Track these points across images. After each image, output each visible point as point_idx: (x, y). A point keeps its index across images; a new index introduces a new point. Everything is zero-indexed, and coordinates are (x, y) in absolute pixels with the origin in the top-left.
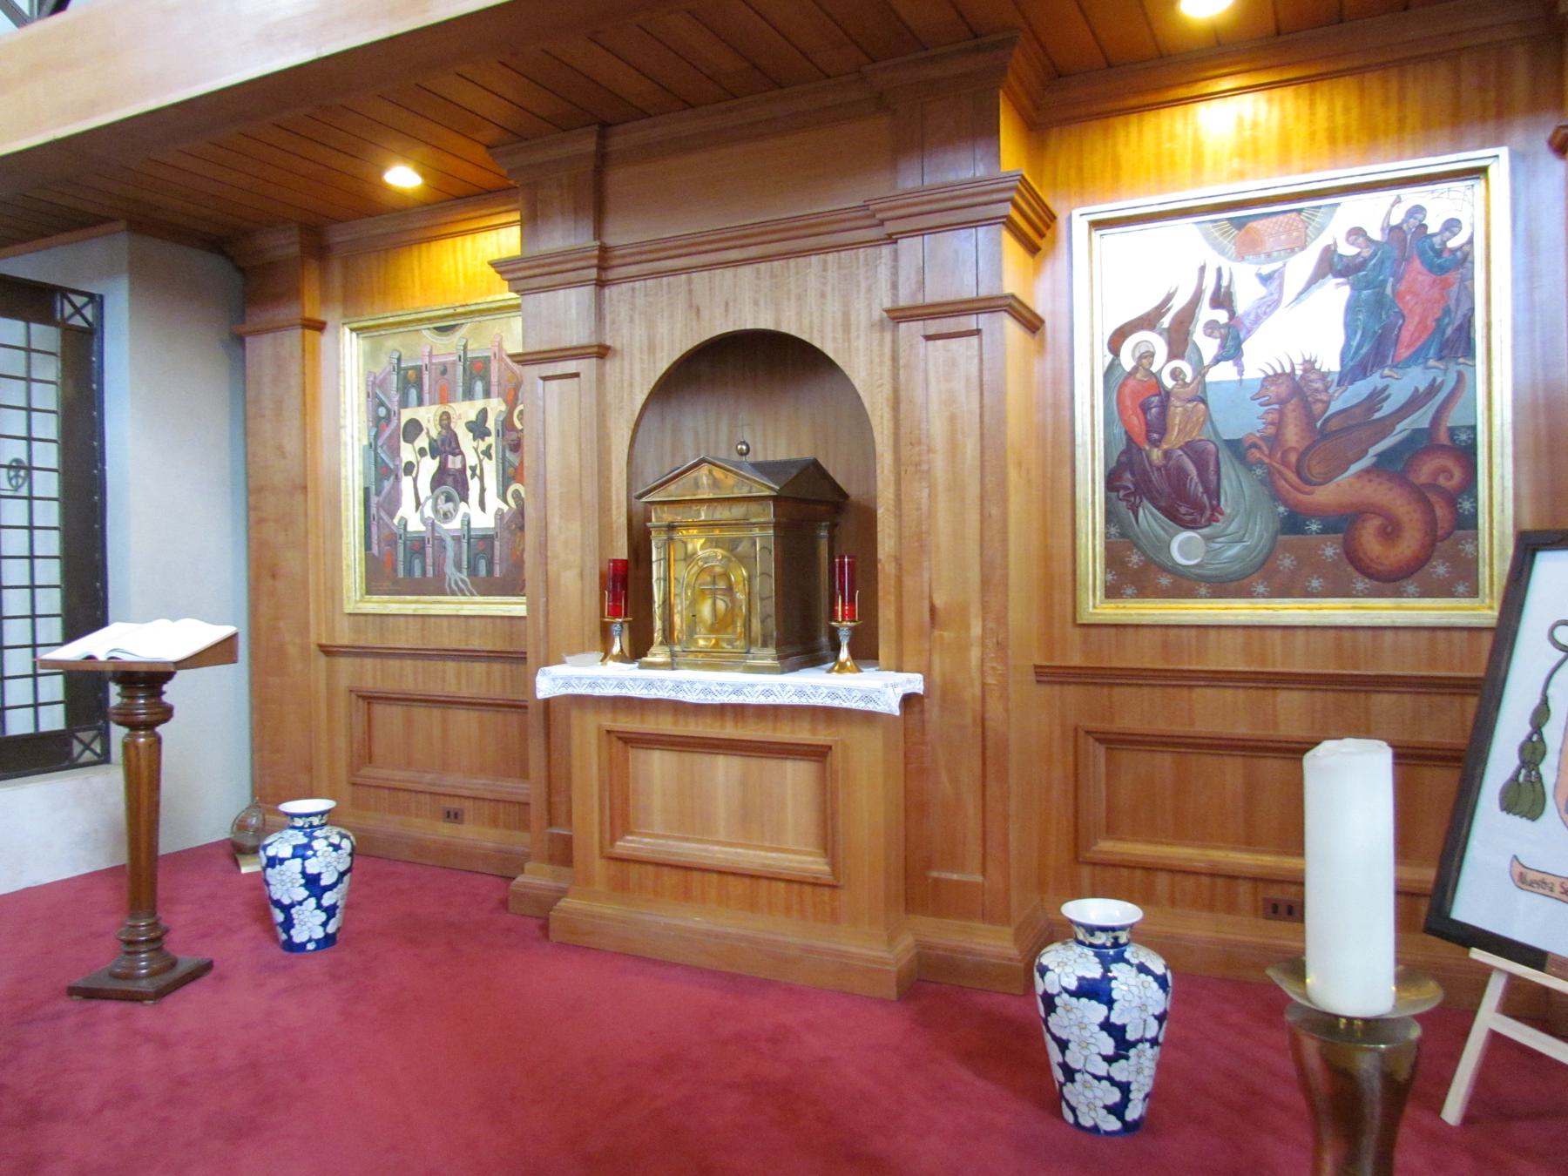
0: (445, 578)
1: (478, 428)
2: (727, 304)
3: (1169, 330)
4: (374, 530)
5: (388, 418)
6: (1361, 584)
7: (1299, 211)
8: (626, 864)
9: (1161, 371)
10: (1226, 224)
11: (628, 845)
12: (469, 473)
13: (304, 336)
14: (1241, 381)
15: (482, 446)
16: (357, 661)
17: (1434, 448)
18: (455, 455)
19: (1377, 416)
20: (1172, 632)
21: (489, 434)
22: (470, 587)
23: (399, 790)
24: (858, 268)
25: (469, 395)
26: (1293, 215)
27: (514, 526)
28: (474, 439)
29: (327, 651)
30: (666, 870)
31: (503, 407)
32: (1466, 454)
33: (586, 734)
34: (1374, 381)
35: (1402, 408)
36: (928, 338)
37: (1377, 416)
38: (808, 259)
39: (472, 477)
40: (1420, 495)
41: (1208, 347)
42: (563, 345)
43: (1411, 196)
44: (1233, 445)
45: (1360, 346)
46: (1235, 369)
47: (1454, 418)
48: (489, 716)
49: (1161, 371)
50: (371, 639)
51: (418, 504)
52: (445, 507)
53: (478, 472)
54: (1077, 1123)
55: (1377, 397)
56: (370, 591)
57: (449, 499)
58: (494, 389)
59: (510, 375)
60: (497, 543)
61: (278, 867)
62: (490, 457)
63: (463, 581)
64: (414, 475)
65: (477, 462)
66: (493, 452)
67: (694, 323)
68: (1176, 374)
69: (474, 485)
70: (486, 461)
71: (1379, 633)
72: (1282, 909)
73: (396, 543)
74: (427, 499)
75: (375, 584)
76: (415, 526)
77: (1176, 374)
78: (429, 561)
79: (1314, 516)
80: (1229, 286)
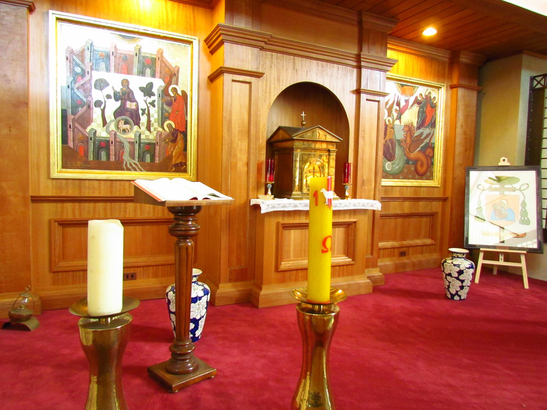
0: (123, 162)
1: (147, 91)
2: (307, 71)
3: (388, 109)
4: (70, 134)
5: (83, 76)
6: (417, 177)
7: (413, 86)
8: (285, 272)
9: (386, 119)
10: (400, 85)
11: (285, 265)
12: (140, 112)
13: (294, 60)
14: (400, 125)
15: (150, 100)
16: (59, 205)
17: (429, 147)
18: (132, 102)
19: (422, 138)
20: (387, 187)
21: (154, 95)
22: (140, 167)
23: (76, 271)
24: (347, 72)
25: (142, 73)
26: (411, 87)
27: (167, 140)
28: (145, 96)
29: (36, 200)
30: (300, 271)
31: (163, 84)
32: (433, 149)
33: (270, 227)
34: (421, 130)
35: (425, 137)
36: (367, 100)
37: (422, 138)
38: (333, 64)
39: (143, 114)
40: (426, 156)
41: (395, 115)
42: (244, 69)
43: (430, 89)
44: (398, 141)
45: (420, 122)
46: (399, 122)
47: (432, 142)
48: (155, 227)
49: (386, 119)
50: (71, 192)
51: (105, 123)
52: (122, 126)
53: (146, 112)
54: (460, 299)
55: (422, 134)
56: (65, 166)
57: (126, 123)
58: (158, 74)
59: (167, 70)
60: (157, 148)
61: (198, 301)
62: (154, 106)
63: (135, 164)
64: (102, 107)
65: (146, 107)
66: (156, 103)
67: (295, 75)
68: (389, 121)
69: (144, 119)
70: (151, 108)
71: (421, 188)
72: (130, 277)
73: (87, 142)
74: (111, 121)
75: (427, 174)
76: (102, 133)
77: (389, 121)
78: (112, 152)
79: (411, 160)
80: (400, 101)
